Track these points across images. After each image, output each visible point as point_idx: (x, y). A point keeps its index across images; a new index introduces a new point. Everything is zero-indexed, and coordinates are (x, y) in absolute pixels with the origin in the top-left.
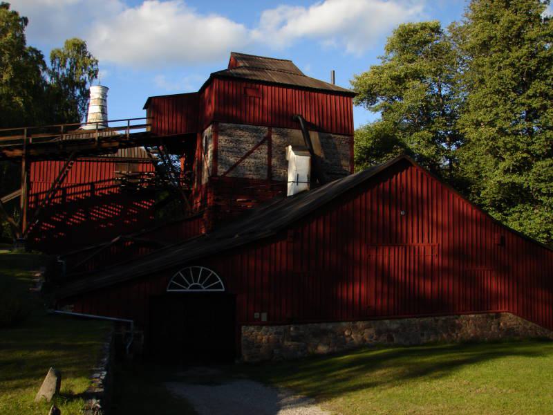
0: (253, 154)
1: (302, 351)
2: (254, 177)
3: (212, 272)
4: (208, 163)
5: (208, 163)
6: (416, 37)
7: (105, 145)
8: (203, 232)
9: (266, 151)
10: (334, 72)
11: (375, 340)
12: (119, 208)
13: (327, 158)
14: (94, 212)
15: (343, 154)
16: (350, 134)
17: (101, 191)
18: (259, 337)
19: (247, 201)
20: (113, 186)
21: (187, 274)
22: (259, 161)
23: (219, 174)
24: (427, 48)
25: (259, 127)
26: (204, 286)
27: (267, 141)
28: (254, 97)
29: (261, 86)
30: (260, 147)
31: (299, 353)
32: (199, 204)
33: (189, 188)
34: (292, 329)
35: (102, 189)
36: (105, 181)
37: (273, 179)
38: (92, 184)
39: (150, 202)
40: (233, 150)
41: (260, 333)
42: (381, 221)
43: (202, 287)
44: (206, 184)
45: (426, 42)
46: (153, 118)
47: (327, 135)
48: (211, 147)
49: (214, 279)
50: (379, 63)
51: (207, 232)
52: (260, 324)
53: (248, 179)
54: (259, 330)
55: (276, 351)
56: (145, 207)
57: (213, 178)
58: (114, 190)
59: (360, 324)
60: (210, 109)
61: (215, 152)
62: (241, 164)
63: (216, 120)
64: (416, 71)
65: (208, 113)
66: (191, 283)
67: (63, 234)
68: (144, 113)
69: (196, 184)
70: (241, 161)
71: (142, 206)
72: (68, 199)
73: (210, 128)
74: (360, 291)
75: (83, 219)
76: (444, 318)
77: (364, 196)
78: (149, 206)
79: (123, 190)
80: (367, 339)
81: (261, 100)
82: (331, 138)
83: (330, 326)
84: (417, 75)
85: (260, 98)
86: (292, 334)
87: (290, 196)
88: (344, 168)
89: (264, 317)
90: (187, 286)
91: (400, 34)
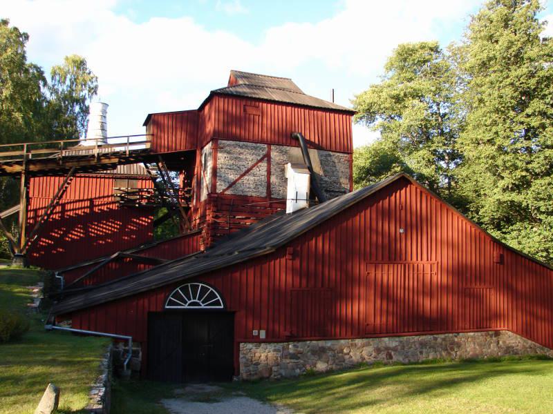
1: (300, 369)
2: (254, 194)
3: (211, 289)
4: (207, 179)
5: (207, 179)
6: (416, 56)
7: (106, 161)
8: (202, 249)
9: (265, 169)
12: (118, 225)
13: (326, 176)
14: (92, 228)
15: (342, 172)
17: (100, 208)
18: (257, 355)
19: (246, 218)
20: (113, 203)
21: (185, 290)
25: (258, 145)
26: (203, 302)
27: (266, 159)
30: (259, 164)
31: (298, 371)
32: (198, 221)
34: (290, 346)
35: (101, 205)
36: (104, 197)
37: (272, 196)
38: (91, 200)
39: (148, 219)
40: (232, 167)
41: (258, 350)
44: (205, 201)
46: (153, 135)
49: (212, 296)
50: (378, 82)
51: (206, 249)
52: (257, 341)
53: (247, 196)
54: (258, 347)
55: (275, 369)
56: (144, 223)
57: (213, 195)
58: (114, 207)
59: (359, 342)
60: (210, 127)
62: (240, 181)
63: (216, 137)
65: (208, 130)
66: (194, 298)
67: (109, 241)
68: (143, 130)
69: (195, 201)
71: (141, 222)
72: (67, 215)
73: (210, 145)
75: (82, 235)
76: (443, 336)
78: (147, 222)
79: (122, 206)
80: (366, 357)
82: (330, 155)
83: (329, 344)
84: (417, 95)
86: (291, 351)
87: (289, 214)
89: (263, 334)
90: (186, 302)
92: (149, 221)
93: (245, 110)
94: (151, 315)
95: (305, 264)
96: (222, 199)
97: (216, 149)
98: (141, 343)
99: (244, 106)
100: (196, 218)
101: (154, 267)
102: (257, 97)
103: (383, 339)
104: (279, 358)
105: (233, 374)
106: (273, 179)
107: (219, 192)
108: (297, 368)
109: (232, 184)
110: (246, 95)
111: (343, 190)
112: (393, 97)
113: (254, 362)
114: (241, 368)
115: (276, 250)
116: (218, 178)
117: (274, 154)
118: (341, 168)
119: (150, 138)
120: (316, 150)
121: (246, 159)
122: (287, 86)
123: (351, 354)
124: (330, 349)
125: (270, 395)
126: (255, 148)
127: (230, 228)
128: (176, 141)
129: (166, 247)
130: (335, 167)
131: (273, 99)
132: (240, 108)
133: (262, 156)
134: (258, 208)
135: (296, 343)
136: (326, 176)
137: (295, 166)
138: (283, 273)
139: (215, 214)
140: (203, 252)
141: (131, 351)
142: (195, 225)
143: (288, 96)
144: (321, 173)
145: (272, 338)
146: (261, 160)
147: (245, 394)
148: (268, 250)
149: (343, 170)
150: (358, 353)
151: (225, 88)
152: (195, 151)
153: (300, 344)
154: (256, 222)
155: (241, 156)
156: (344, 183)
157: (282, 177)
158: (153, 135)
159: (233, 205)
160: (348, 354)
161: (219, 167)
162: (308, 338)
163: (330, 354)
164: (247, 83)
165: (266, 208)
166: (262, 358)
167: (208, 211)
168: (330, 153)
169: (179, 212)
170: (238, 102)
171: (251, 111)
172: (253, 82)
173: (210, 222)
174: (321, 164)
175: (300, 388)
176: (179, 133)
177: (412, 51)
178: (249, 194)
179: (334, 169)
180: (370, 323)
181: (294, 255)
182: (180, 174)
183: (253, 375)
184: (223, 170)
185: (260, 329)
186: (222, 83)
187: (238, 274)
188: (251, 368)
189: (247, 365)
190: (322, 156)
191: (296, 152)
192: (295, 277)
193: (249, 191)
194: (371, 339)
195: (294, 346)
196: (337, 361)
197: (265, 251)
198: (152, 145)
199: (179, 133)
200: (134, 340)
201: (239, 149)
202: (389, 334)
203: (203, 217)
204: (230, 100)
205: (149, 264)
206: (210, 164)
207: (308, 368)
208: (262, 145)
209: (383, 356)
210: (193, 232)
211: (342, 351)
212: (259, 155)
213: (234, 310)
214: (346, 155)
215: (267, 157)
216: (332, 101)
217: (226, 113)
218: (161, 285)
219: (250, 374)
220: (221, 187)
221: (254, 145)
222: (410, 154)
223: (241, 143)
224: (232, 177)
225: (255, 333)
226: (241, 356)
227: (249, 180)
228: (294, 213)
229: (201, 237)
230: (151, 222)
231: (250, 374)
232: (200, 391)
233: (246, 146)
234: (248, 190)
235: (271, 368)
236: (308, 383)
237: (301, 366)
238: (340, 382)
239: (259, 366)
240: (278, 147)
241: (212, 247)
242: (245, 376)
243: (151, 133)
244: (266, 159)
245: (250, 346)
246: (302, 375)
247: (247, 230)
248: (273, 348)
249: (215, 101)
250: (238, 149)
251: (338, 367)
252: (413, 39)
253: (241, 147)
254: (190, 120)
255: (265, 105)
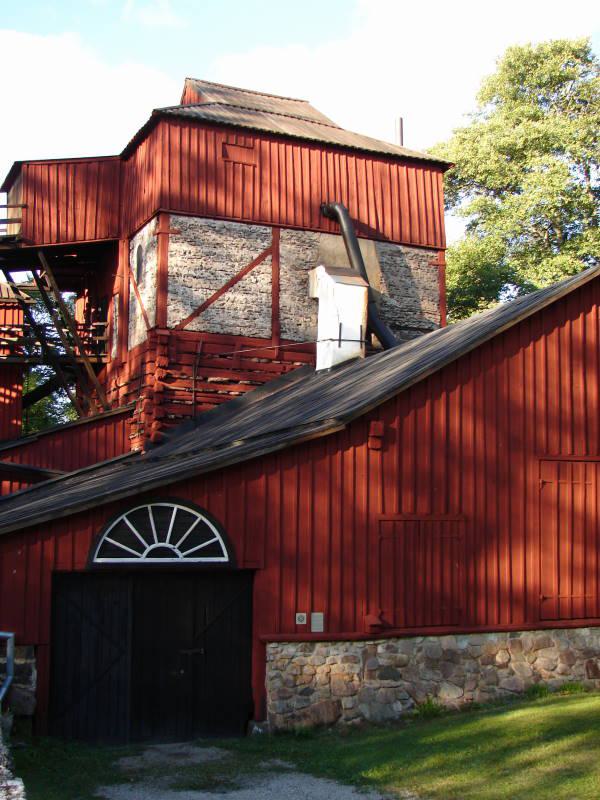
0: (240, 283)
1: (403, 701)
2: (245, 332)
3: (200, 517)
4: (144, 299)
5: (144, 299)
6: (546, 70)
8: (136, 447)
9: (268, 278)
10: (401, 119)
11: (562, 674)
13: (392, 296)
15: (425, 289)
16: (439, 246)
18: (307, 670)
19: (230, 382)
21: (140, 520)
22: (254, 297)
23: (170, 324)
24: (567, 90)
25: (254, 227)
26: (182, 549)
27: (269, 257)
28: (244, 164)
29: (257, 141)
31: (398, 707)
32: (123, 391)
33: (100, 358)
34: (380, 649)
37: (284, 336)
39: (12, 390)
40: (198, 274)
41: (309, 659)
42: (567, 407)
43: (177, 552)
44: (142, 346)
45: (560, 81)
46: (25, 207)
47: (394, 247)
48: (152, 265)
49: (203, 532)
50: (466, 123)
51: (147, 446)
52: (306, 638)
53: (230, 334)
54: (307, 651)
55: (346, 702)
57: (159, 332)
59: (528, 637)
60: (151, 187)
61: (163, 278)
62: (216, 304)
63: (168, 207)
64: (546, 138)
65: (145, 196)
66: (151, 542)
69: (114, 348)
70: (215, 297)
73: (151, 226)
74: (522, 567)
77: (530, 348)
78: (10, 397)
80: (544, 673)
81: (257, 170)
82: (399, 253)
83: (463, 643)
84: (547, 145)
85: (255, 166)
86: (382, 661)
87: (324, 371)
88: (427, 316)
89: (318, 623)
90: (141, 549)
91: (510, 65)
92: (14, 395)
93: (225, 154)
94: (66, 581)
95: (408, 459)
96: (178, 339)
97: (162, 238)
98: (36, 647)
99: (224, 144)
100: (120, 384)
101: (32, 486)
102: (251, 126)
103: (577, 631)
104: (356, 678)
105: (251, 716)
106: (285, 299)
107: (173, 325)
108: (397, 699)
109: (200, 310)
110: (227, 122)
111: (195, 339)
112: (501, 150)
113: (300, 688)
114: (270, 701)
115: (349, 426)
116: (170, 296)
117: (285, 248)
118: (423, 276)
119: (19, 213)
120: (371, 241)
121: (229, 257)
122: (301, 111)
123: (512, 665)
124: (466, 654)
125: (368, 766)
126: (248, 235)
127: (198, 403)
128: (83, 223)
129: (58, 443)
130: (410, 277)
131: (282, 132)
132: (210, 150)
133: (260, 251)
134: (255, 360)
135: (391, 643)
136: (392, 296)
137: (333, 270)
138: (365, 480)
139: (164, 373)
140: (139, 453)
141: (11, 669)
142: (116, 400)
143: (316, 133)
144: (383, 290)
145: (337, 632)
146: (262, 258)
147: (294, 766)
148: (330, 427)
149: (428, 285)
150: (527, 664)
151: (177, 108)
152: (117, 243)
153: (401, 644)
154: (251, 390)
155: (218, 251)
156: (429, 307)
157: (303, 296)
158: (25, 207)
159: (202, 354)
160: (505, 666)
161: (166, 274)
162: (417, 631)
163: (467, 666)
164: (224, 102)
165: (270, 361)
166: (318, 677)
167: (148, 366)
168: (401, 247)
169: (78, 372)
170: (211, 135)
171: (236, 154)
172: (236, 101)
173: (155, 388)
174: (383, 270)
175: (431, 749)
176: (80, 205)
177: (535, 60)
178: (236, 331)
179: (408, 281)
180: (548, 596)
181: (385, 441)
182: (79, 297)
183: (299, 718)
184: (181, 279)
185: (313, 610)
186: (171, 100)
187: (50, 545)
188: (294, 703)
189: (283, 696)
190: (383, 253)
191: (333, 244)
192: (386, 489)
193: (234, 325)
194: (553, 632)
195: (388, 648)
196: (482, 683)
197: (323, 431)
198: (23, 229)
199: (80, 205)
200: (18, 643)
201: (214, 236)
202: (591, 621)
203: (137, 380)
204: (195, 132)
205: (22, 481)
206: (152, 265)
207: (422, 698)
208: (261, 229)
209: (579, 669)
210: (115, 411)
211: (491, 660)
212: (256, 249)
213: (249, 566)
214: (431, 254)
215: (273, 252)
216: (399, 144)
217: (185, 156)
218: (84, 508)
219: (293, 717)
220: (177, 314)
221: (245, 227)
222: (537, 263)
223: (219, 223)
224: (200, 295)
225: (301, 618)
226: (270, 673)
227: (235, 299)
228: (335, 368)
229: (135, 422)
230: (17, 397)
231: (293, 717)
232: (181, 762)
233: (228, 230)
234: (232, 322)
235: (339, 702)
236: (442, 736)
237: (405, 695)
238: (519, 733)
239: (311, 698)
240: (294, 232)
241: (158, 442)
242: (279, 721)
243: (21, 202)
244: (269, 257)
245: (291, 649)
246: (409, 717)
247: (234, 406)
248: (342, 655)
249: (163, 131)
250: (212, 236)
251: (486, 696)
252: (537, 36)
253: (218, 232)
254: (108, 178)
255: (266, 144)
